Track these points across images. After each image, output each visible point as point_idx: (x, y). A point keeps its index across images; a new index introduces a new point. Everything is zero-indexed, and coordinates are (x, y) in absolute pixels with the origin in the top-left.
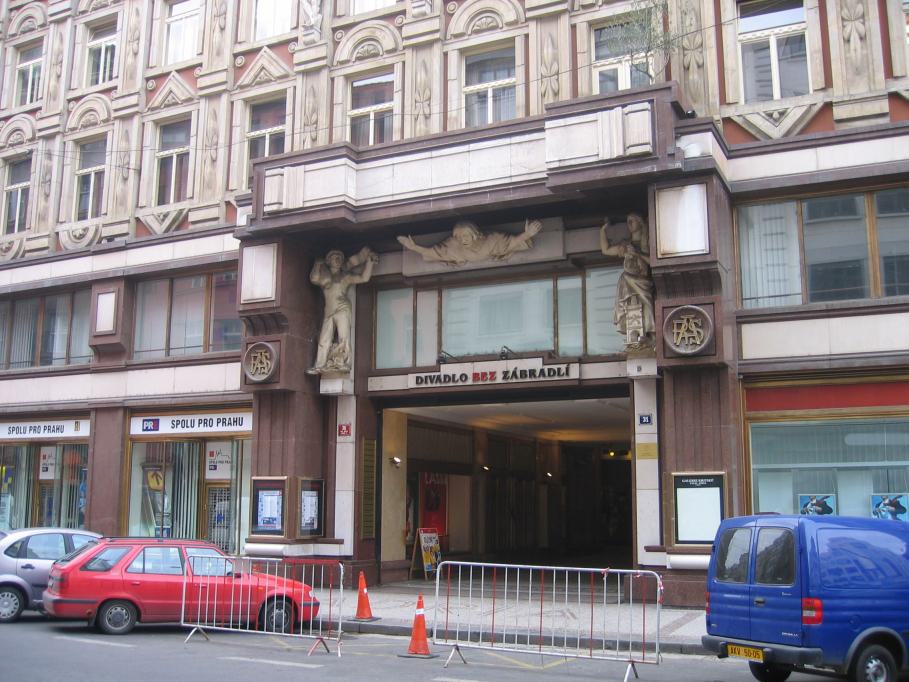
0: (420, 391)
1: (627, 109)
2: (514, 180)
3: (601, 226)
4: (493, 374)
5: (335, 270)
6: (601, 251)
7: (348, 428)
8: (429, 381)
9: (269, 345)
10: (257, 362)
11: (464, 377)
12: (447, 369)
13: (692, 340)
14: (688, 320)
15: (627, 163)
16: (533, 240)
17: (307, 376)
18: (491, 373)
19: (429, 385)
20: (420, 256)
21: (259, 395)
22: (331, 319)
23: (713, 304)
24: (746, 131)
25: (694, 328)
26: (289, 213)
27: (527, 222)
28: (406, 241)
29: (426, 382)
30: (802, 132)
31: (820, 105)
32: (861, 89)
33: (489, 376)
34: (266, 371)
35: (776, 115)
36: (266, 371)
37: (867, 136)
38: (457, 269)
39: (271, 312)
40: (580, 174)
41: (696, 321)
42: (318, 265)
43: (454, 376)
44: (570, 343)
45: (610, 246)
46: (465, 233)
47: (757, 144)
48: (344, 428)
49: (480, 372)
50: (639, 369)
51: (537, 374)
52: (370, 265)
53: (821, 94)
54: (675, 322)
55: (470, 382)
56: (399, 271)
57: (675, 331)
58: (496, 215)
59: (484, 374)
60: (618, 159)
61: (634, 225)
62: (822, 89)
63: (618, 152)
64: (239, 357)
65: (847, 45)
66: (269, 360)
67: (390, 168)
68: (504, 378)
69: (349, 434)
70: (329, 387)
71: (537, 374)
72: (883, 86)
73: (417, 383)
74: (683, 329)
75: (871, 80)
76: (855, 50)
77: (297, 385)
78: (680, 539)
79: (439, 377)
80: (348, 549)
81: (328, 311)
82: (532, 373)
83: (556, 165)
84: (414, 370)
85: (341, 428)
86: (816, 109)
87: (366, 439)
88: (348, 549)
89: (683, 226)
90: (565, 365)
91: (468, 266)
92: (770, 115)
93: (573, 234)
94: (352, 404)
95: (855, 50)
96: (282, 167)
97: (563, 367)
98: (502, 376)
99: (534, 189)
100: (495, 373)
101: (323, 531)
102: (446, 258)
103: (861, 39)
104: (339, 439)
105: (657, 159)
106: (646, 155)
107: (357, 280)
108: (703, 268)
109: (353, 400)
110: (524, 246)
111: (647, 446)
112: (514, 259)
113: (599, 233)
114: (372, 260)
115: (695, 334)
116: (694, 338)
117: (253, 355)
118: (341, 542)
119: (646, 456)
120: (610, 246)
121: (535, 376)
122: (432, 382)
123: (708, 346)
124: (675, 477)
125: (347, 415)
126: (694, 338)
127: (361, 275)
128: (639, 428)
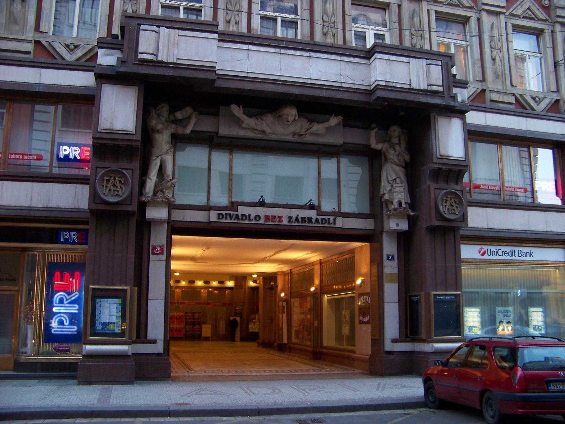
0: (219, 225)
2: (343, 85)
4: (280, 217)
6: (370, 145)
7: (161, 249)
10: (110, 185)
11: (258, 217)
12: (242, 210)
13: (116, 193)
14: (451, 199)
16: (329, 129)
19: (228, 221)
20: (238, 122)
22: (159, 158)
23: (133, 169)
24: (49, 52)
27: (333, 115)
28: (237, 110)
29: (226, 218)
30: (88, 60)
33: (277, 219)
34: (120, 193)
35: (72, 47)
41: (120, 179)
43: (250, 215)
45: (378, 142)
46: (291, 112)
47: (54, 61)
48: (158, 248)
49: (306, 217)
50: (397, 225)
52: (193, 120)
54: (106, 178)
55: (262, 221)
58: (314, 103)
61: (397, 133)
64: (88, 180)
65: (227, 24)
67: (246, 52)
68: (289, 221)
69: (161, 253)
70: (153, 213)
71: (314, 221)
72: (31, 35)
73: (219, 218)
74: (448, 204)
77: (134, 207)
79: (237, 215)
80: (159, 348)
81: (156, 151)
82: (310, 220)
83: (384, 84)
85: (154, 248)
87: (321, 262)
90: (333, 217)
91: (273, 137)
92: (68, 46)
96: (159, 27)
97: (332, 218)
98: (288, 220)
101: (140, 334)
103: (236, 23)
104: (152, 257)
107: (180, 131)
108: (129, 143)
109: (166, 225)
111: (391, 275)
112: (308, 139)
115: (119, 188)
117: (106, 178)
118: (154, 342)
119: (391, 281)
121: (312, 222)
123: (125, 199)
124: (434, 294)
126: (118, 191)
127: (185, 127)
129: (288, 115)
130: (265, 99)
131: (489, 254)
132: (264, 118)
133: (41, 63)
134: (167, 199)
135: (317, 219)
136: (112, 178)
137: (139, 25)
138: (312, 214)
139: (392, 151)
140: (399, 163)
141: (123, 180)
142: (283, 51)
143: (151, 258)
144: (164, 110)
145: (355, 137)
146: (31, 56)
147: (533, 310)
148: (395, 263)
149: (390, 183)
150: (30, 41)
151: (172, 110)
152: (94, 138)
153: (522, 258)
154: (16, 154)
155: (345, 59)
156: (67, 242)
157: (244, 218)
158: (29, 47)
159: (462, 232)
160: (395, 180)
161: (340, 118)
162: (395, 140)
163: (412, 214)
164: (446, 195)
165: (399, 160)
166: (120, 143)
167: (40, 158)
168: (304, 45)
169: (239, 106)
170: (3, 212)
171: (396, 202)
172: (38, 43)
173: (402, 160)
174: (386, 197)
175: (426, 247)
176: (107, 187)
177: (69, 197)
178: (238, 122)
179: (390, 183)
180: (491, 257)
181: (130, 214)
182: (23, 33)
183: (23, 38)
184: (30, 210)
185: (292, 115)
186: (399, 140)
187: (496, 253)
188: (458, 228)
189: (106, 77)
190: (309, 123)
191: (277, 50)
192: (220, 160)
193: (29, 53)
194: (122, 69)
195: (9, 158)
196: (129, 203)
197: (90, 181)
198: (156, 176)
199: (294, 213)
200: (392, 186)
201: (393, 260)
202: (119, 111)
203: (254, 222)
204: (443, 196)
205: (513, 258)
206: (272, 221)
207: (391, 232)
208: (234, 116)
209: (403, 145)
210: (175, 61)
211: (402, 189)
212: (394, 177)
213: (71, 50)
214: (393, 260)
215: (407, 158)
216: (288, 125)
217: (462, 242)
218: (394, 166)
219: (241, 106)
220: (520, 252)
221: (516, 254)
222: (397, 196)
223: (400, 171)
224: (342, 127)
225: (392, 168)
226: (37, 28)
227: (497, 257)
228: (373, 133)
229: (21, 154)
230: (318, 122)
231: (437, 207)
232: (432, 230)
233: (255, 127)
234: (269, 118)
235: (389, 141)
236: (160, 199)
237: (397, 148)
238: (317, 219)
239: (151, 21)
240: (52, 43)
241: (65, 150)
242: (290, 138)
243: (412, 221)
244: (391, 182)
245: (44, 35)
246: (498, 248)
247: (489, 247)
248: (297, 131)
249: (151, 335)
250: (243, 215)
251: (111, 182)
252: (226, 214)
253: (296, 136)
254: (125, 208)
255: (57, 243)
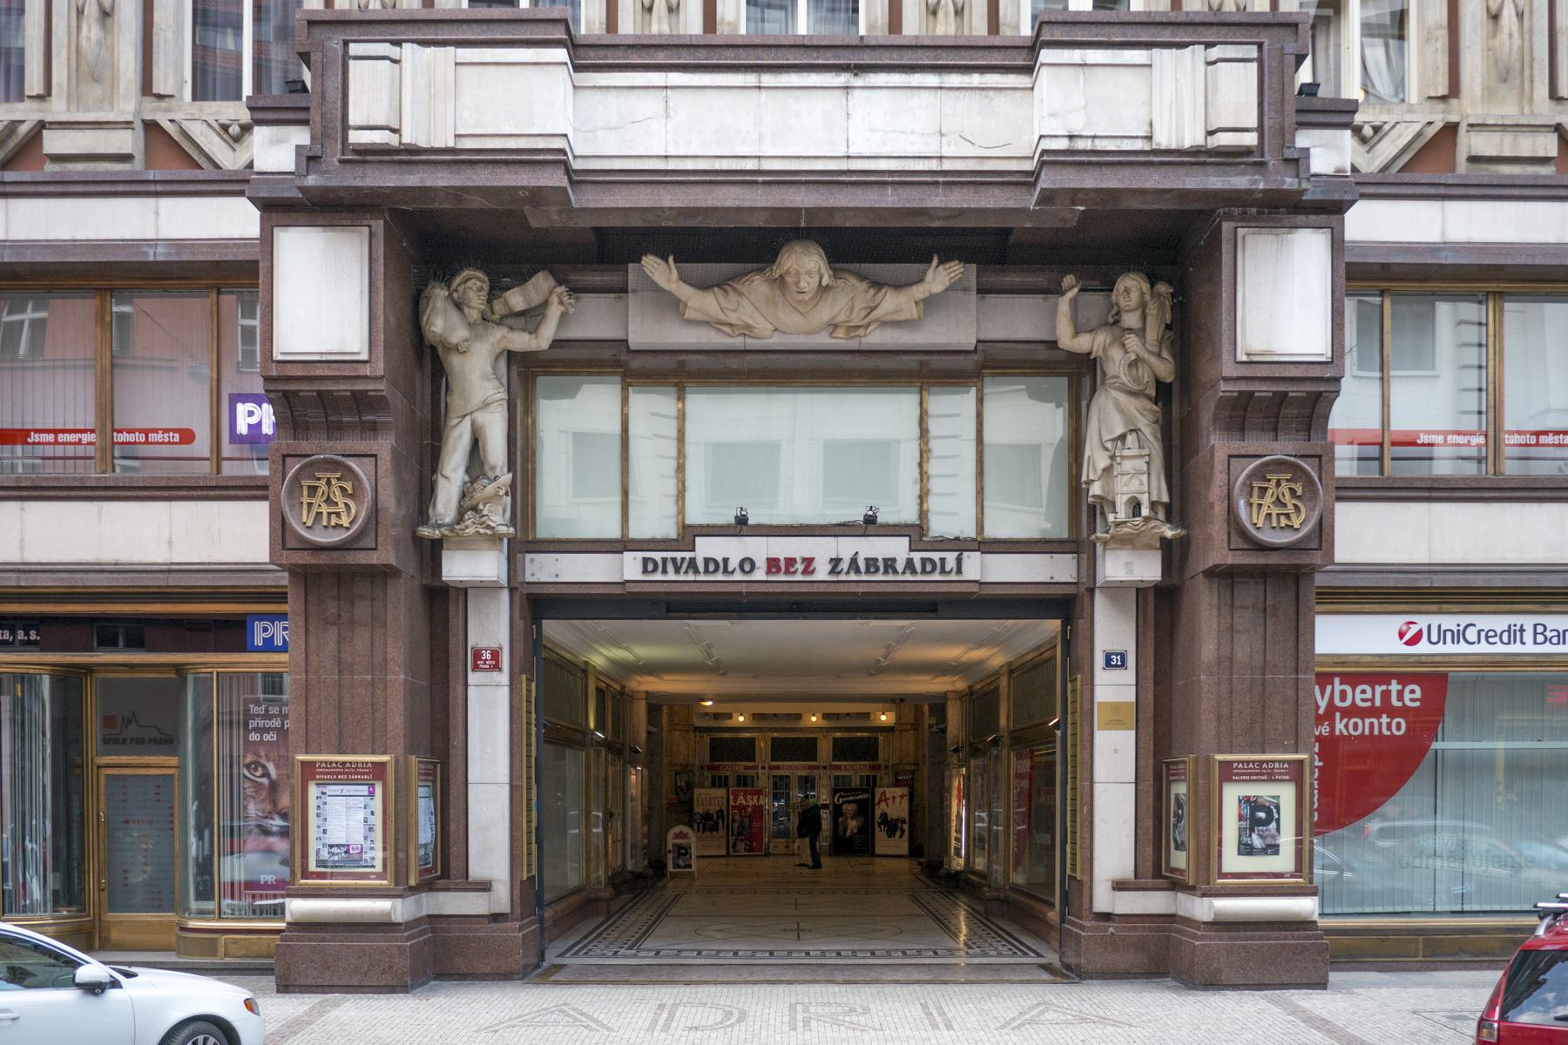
1: (1215, 53)
2: (947, 166)
3: (1061, 293)
4: (808, 561)
5: (474, 315)
7: (496, 655)
8: (670, 568)
9: (352, 463)
10: (318, 500)
11: (748, 564)
12: (706, 548)
13: (1284, 522)
14: (1278, 484)
15: (1204, 164)
16: (930, 304)
17: (418, 541)
18: (804, 560)
19: (671, 576)
20: (675, 305)
21: (307, 577)
23: (1320, 457)
25: (1287, 499)
26: (410, 156)
27: (935, 261)
28: (659, 270)
29: (665, 571)
31: (1439, 125)
32: (1508, 110)
33: (800, 567)
34: (345, 521)
35: (234, 130)
36: (345, 521)
37: (1526, 192)
38: (752, 343)
39: (359, 386)
40: (859, 191)
42: (439, 294)
43: (726, 561)
44: (952, 516)
45: (1077, 333)
51: (900, 566)
52: (554, 312)
53: (1440, 106)
54: (306, 483)
55: (759, 575)
56: (618, 335)
57: (1255, 500)
58: (876, 235)
59: (790, 562)
60: (1196, 151)
62: (1443, 98)
63: (1192, 137)
64: (266, 488)
66: (351, 496)
68: (832, 572)
69: (497, 667)
70: (458, 567)
71: (900, 566)
73: (645, 571)
74: (1269, 499)
75: (1526, 96)
76: (1511, 36)
78: (1226, 869)
79: (693, 561)
82: (890, 564)
83: (1063, 144)
84: (622, 545)
85: (477, 654)
86: (1431, 132)
88: (501, 898)
89: (1282, 303)
91: (776, 341)
92: (225, 128)
93: (992, 299)
94: (502, 604)
95: (1511, 36)
96: (398, 43)
97: (951, 558)
98: (829, 568)
99: (996, 191)
100: (812, 560)
101: (446, 865)
102: (733, 318)
104: (473, 678)
105: (1263, 164)
106: (1246, 151)
107: (521, 341)
109: (505, 595)
110: (913, 312)
111: (1116, 707)
112: (877, 338)
113: (1056, 305)
114: (561, 303)
116: (1288, 516)
119: (1115, 724)
120: (1077, 333)
121: (895, 572)
122: (677, 570)
124: (303, 763)
125: (492, 627)
126: (338, 515)
127: (534, 331)
128: (1102, 676)
129: (798, 274)
130: (729, 235)
131: (1434, 639)
132: (744, 289)
133: (155, 182)
134: (488, 527)
135: (910, 563)
136: (323, 482)
137: (346, 43)
138: (898, 548)
139: (1116, 354)
140: (1135, 387)
141: (348, 486)
142: (768, 79)
143: (470, 681)
144: (473, 284)
145: (1016, 320)
146: (138, 164)
147: (377, 803)
148: (1128, 676)
149: (1106, 449)
150: (127, 125)
151: (496, 290)
152: (267, 379)
153: (1548, 648)
154: (129, 431)
155: (954, 79)
156: (269, 646)
157: (929, 568)
158: (124, 141)
159: (1320, 580)
160: (1123, 437)
161: (955, 269)
162: (1131, 320)
163: (1169, 533)
164: (1260, 474)
165: (1137, 380)
166: (331, 387)
167: (187, 436)
168: (829, 53)
169: (666, 260)
170: (11, 581)
171: (1121, 501)
172: (151, 127)
173: (1146, 376)
174: (1096, 489)
175: (1208, 624)
176: (310, 505)
177: (233, 536)
178: (675, 305)
179: (1106, 449)
180: (1440, 649)
181: (382, 575)
182: (112, 104)
183: (111, 117)
184: (169, 571)
185: (809, 273)
186: (1144, 318)
187: (1460, 635)
188: (1312, 570)
189: (282, 208)
190: (872, 292)
191: (750, 79)
192: (651, 410)
193: (126, 158)
194: (312, 180)
195: (113, 443)
196: (288, 545)
197: (270, 493)
198: (462, 470)
199: (847, 547)
200: (1113, 458)
201: (1123, 665)
202: (323, 300)
203: (738, 576)
204: (1251, 476)
205: (1516, 648)
206: (787, 572)
207: (1116, 590)
208: (656, 288)
209: (1152, 333)
210: (451, 144)
211: (1141, 464)
212: (1119, 431)
213: (237, 139)
214: (1123, 665)
215: (1165, 369)
216: (802, 303)
217: (1318, 608)
218: (1122, 397)
219: (671, 259)
220: (1540, 629)
221: (1528, 636)
222: (1126, 484)
223: (1143, 416)
224: (973, 295)
225: (1117, 404)
226: (146, 87)
227: (1462, 648)
228: (1064, 304)
229: (141, 431)
230: (898, 286)
231: (1231, 510)
232: (1226, 576)
233: (722, 317)
234: (758, 286)
235: (1113, 321)
236: (471, 531)
237: (1132, 341)
238: (910, 563)
239: (381, 28)
240: (185, 125)
241: (251, 414)
242: (824, 340)
243: (1174, 554)
244: (1109, 445)
245: (163, 104)
246: (1464, 620)
247: (1435, 620)
248: (842, 318)
249: (478, 868)
250: (707, 561)
251: (320, 492)
252: (664, 560)
253: (840, 333)
254: (361, 558)
255: (245, 651)
